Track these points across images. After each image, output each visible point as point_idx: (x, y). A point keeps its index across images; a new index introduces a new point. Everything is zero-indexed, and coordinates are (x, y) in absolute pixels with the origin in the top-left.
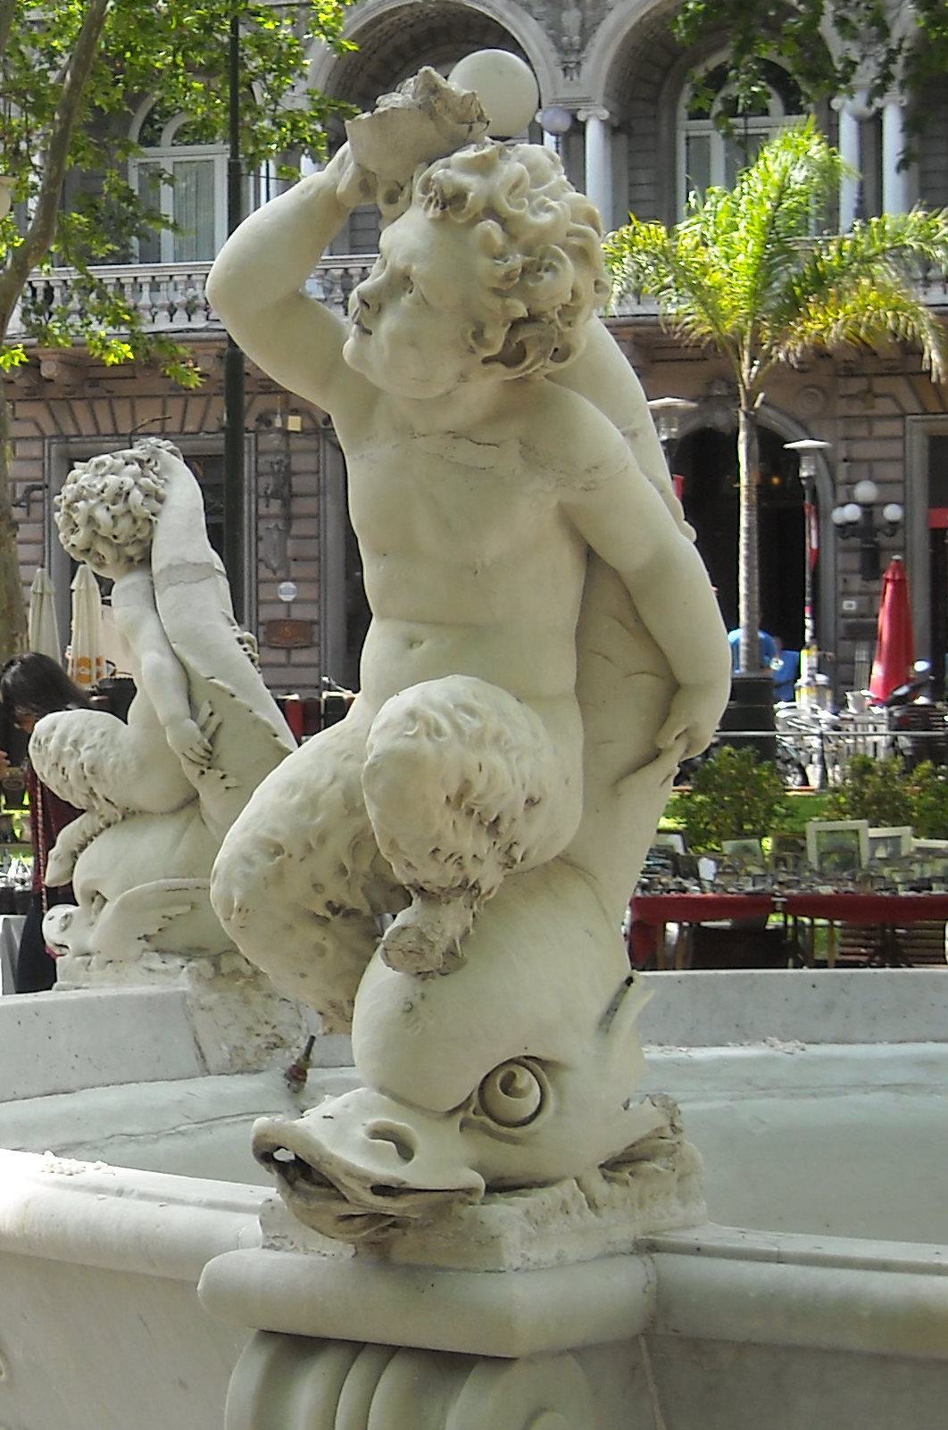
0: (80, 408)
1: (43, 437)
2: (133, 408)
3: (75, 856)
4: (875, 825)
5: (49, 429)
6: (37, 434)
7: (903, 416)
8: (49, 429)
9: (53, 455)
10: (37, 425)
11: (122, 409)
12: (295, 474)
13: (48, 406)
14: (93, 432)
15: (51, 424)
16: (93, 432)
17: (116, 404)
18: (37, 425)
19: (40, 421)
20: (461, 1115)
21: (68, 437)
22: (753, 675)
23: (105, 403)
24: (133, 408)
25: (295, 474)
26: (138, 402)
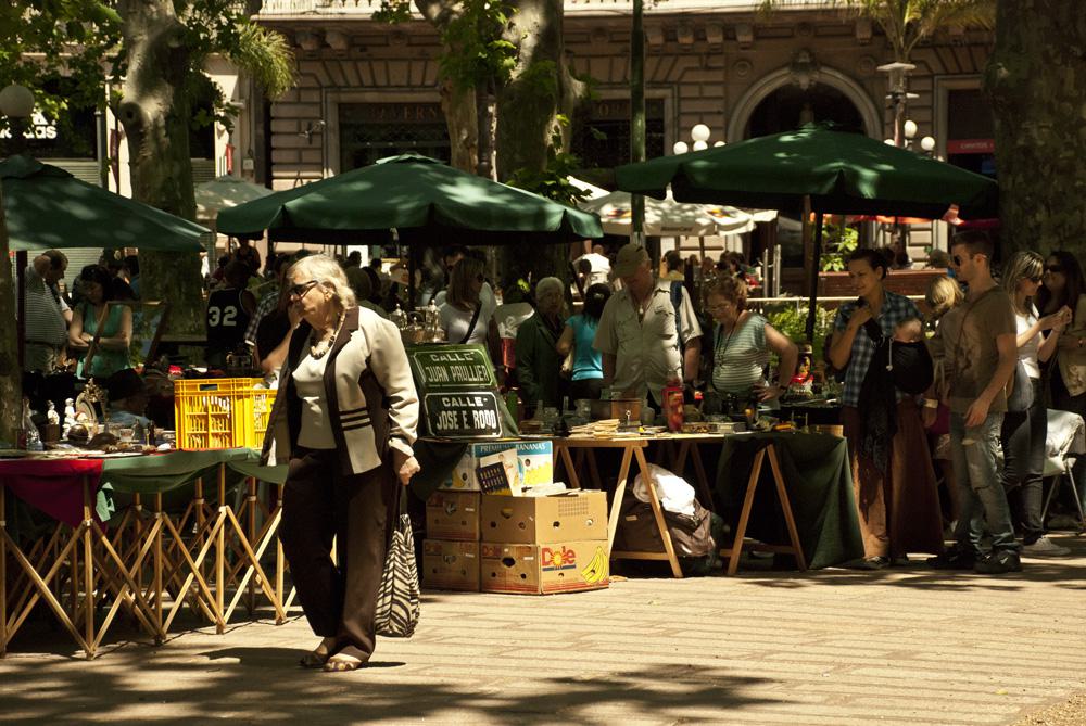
0: (348, 67)
1: (321, 87)
2: (387, 67)
3: (965, 672)
4: (524, 434)
5: (325, 82)
6: (318, 86)
7: (931, 76)
8: (325, 82)
9: (329, 100)
10: (316, 78)
11: (379, 68)
12: (273, 118)
13: (324, 65)
14: (357, 84)
15: (369, 77)
16: (357, 84)
17: (375, 64)
18: (316, 78)
19: (318, 74)
20: (1052, 212)
21: (339, 87)
22: (480, 248)
23: (366, 64)
24: (387, 67)
25: (273, 118)
26: (391, 64)
